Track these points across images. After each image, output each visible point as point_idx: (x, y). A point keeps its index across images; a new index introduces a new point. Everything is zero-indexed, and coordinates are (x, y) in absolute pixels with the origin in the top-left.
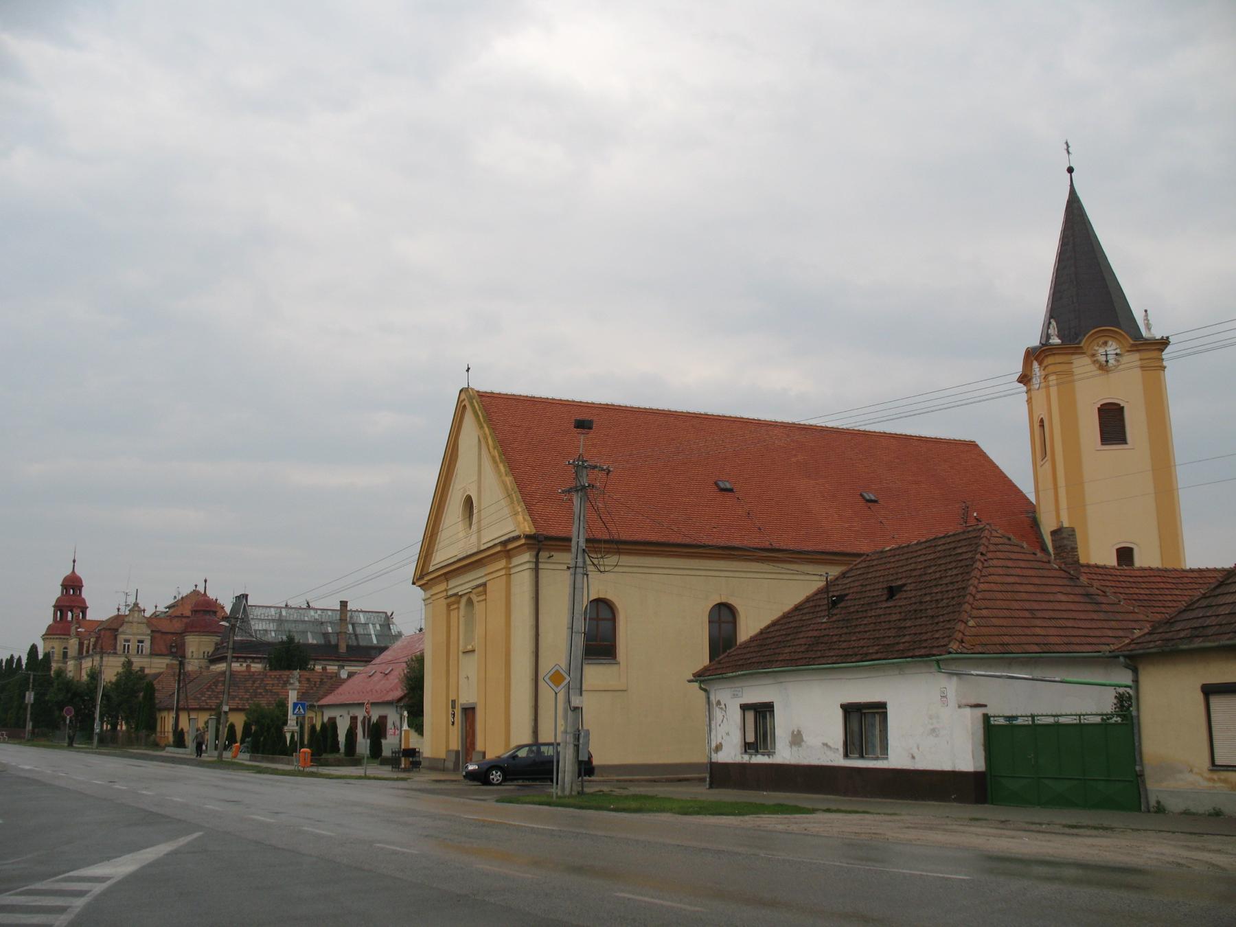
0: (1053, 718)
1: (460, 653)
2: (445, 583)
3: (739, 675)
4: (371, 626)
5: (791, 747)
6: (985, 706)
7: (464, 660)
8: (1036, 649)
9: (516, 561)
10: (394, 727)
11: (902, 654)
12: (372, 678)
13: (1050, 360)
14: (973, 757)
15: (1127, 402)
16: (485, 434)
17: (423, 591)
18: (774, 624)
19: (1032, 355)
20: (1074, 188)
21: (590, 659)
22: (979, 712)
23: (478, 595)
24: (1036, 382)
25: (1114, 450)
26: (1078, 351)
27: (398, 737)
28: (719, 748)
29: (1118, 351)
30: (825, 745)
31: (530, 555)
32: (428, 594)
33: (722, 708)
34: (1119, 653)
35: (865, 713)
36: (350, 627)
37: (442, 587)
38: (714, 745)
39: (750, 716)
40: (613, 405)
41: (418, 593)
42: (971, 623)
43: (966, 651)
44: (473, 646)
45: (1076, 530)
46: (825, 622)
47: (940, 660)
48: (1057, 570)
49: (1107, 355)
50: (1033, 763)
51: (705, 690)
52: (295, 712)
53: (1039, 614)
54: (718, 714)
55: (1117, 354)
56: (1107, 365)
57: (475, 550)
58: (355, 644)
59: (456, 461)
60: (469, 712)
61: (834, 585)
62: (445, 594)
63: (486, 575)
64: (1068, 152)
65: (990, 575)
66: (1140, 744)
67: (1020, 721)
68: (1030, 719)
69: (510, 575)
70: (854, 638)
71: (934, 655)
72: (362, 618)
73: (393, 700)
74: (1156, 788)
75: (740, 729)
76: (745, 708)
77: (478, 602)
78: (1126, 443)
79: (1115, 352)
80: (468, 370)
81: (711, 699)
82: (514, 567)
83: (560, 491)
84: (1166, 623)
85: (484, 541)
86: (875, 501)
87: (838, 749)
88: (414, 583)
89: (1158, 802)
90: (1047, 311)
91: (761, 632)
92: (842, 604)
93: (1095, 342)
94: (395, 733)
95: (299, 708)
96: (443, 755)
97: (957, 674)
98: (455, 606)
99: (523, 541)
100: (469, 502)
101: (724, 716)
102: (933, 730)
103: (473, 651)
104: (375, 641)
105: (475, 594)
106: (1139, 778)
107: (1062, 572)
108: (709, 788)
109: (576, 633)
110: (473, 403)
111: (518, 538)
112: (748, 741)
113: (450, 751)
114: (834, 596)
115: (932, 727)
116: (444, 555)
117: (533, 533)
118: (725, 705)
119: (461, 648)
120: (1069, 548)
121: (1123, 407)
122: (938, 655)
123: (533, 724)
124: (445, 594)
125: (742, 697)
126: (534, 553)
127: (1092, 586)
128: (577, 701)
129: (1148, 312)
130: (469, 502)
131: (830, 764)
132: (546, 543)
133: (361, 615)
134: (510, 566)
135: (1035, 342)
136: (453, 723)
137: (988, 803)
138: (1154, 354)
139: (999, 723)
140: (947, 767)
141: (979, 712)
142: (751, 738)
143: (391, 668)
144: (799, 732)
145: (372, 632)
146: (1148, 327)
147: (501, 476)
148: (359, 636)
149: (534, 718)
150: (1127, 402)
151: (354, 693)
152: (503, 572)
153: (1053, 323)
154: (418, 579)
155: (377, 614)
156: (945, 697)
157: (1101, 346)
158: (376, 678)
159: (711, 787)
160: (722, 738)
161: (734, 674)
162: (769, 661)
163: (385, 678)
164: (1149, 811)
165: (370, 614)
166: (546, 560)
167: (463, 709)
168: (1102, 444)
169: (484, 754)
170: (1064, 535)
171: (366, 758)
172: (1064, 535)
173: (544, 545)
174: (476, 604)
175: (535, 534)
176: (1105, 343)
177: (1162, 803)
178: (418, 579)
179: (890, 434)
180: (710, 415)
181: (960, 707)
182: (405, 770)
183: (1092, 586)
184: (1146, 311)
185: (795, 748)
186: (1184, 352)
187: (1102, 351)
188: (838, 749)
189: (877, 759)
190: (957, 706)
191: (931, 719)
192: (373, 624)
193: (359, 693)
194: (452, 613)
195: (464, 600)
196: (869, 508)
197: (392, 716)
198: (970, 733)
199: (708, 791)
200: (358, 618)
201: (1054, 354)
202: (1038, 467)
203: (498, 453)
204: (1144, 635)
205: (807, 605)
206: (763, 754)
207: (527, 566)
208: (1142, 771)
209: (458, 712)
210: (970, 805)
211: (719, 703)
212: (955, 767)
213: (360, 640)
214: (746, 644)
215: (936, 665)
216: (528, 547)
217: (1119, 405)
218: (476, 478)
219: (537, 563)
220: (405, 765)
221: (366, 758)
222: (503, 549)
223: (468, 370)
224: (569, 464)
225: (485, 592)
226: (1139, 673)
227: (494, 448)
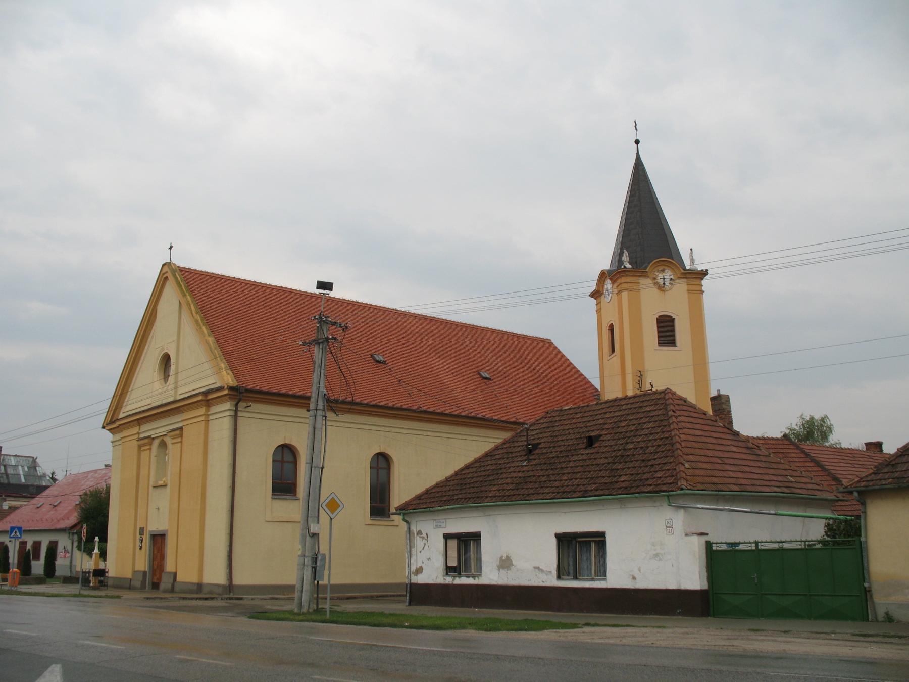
0: (778, 544)
1: (151, 488)
2: (138, 427)
3: (448, 509)
4: (20, 468)
5: (499, 570)
6: (707, 534)
7: (154, 493)
8: (737, 488)
9: (215, 409)
10: (65, 550)
11: (627, 490)
12: (40, 509)
13: (623, 280)
14: (700, 578)
15: (677, 315)
16: (189, 301)
17: (112, 435)
18: (467, 467)
19: (603, 275)
21: (277, 495)
22: (704, 539)
23: (173, 438)
24: (606, 298)
25: (667, 350)
26: (644, 275)
27: (69, 560)
28: (419, 571)
29: (672, 277)
30: (538, 568)
31: (231, 404)
32: (118, 436)
33: (423, 538)
34: (854, 489)
35: (579, 541)
36: (2, 468)
37: (135, 430)
38: (414, 568)
39: (453, 544)
40: (286, 288)
41: (108, 436)
42: (687, 465)
43: (692, 488)
44: (164, 482)
45: (730, 398)
46: (525, 466)
47: (671, 495)
48: (722, 427)
49: (664, 279)
50: (756, 582)
51: (407, 522)
52: (12, 536)
53: (726, 461)
54: (419, 542)
55: (671, 279)
56: (664, 287)
57: (171, 399)
58: (6, 482)
59: (153, 324)
60: (159, 539)
61: (520, 436)
62: (136, 437)
64: (636, 129)
65: (684, 428)
66: (868, 565)
67: (742, 547)
68: (754, 545)
69: (208, 421)
70: (566, 478)
71: (664, 491)
72: (13, 462)
73: (66, 527)
74: (882, 601)
75: (443, 555)
76: (447, 537)
77: (173, 443)
78: (675, 346)
79: (670, 278)
80: (171, 248)
81: (411, 529)
82: (213, 414)
83: (301, 342)
84: (887, 465)
85: (181, 391)
86: (489, 379)
87: (551, 572)
88: (103, 427)
89: (887, 614)
90: (616, 245)
91: (456, 474)
92: (537, 451)
93: (656, 269)
94: (65, 557)
95: (16, 532)
96: (128, 574)
97: (683, 507)
98: (148, 447)
99: (226, 392)
100: (166, 360)
101: (425, 544)
102: (656, 555)
103: (165, 486)
104: (23, 480)
105: (170, 437)
106: (868, 593)
107: (726, 429)
108: (409, 606)
109: (315, 467)
110: (176, 275)
111: (221, 389)
112: (449, 565)
113: (137, 571)
114: (530, 445)
115: (655, 552)
116: (135, 403)
117: (235, 385)
118: (427, 534)
119: (151, 483)
120: (726, 411)
121: (674, 319)
122: (670, 491)
123: (228, 550)
124: (136, 437)
125: (445, 527)
126: (234, 403)
127: (749, 442)
128: (316, 529)
129: (693, 250)
130: (166, 360)
131: (541, 584)
132: (245, 394)
133: (12, 458)
134: (209, 413)
135: (606, 266)
136: (141, 548)
137: (711, 616)
138: (696, 282)
139: (722, 549)
140: (672, 586)
141: (704, 539)
142: (453, 562)
143: (59, 501)
144: (508, 558)
145: (21, 472)
146: (692, 261)
147: (204, 337)
148: (10, 476)
149: (229, 544)
150: (677, 315)
151: (23, 521)
152: (202, 418)
153: (626, 252)
154: (109, 424)
155: (26, 458)
156: (671, 527)
157: (660, 273)
158: (44, 510)
159: (410, 604)
160: (423, 563)
161: (443, 508)
162: (478, 497)
163: (54, 509)
164: (877, 621)
165: (20, 458)
166: (244, 410)
167: (151, 535)
168: (659, 345)
169: (175, 575)
170: (723, 401)
172: (723, 401)
173: (243, 396)
174: (170, 446)
175: (237, 386)
176: (663, 271)
177: (890, 613)
178: (109, 424)
179: (491, 329)
180: (360, 303)
181: (686, 535)
182: (94, 588)
183: (749, 442)
184: (691, 250)
185: (503, 572)
186: (899, 246)
187: (660, 276)
188: (551, 572)
189: (593, 580)
190: (684, 534)
191: (654, 546)
192: (22, 466)
193: (28, 521)
194: (143, 453)
195: (156, 442)
196: (486, 384)
197: (64, 542)
198: (697, 557)
199: (407, 607)
200: (10, 461)
202: (605, 360)
203: (200, 317)
204: (870, 475)
205: (497, 452)
206: (468, 577)
207: (228, 413)
208: (870, 587)
210: (695, 618)
211: (420, 533)
212: (680, 586)
213: (10, 479)
215: (667, 500)
216: (230, 397)
217: (671, 317)
218: (175, 338)
219: (236, 411)
220: (95, 583)
222: (204, 398)
223: (171, 248)
224: (315, 318)
225: (181, 436)
226: (867, 505)
227: (197, 313)
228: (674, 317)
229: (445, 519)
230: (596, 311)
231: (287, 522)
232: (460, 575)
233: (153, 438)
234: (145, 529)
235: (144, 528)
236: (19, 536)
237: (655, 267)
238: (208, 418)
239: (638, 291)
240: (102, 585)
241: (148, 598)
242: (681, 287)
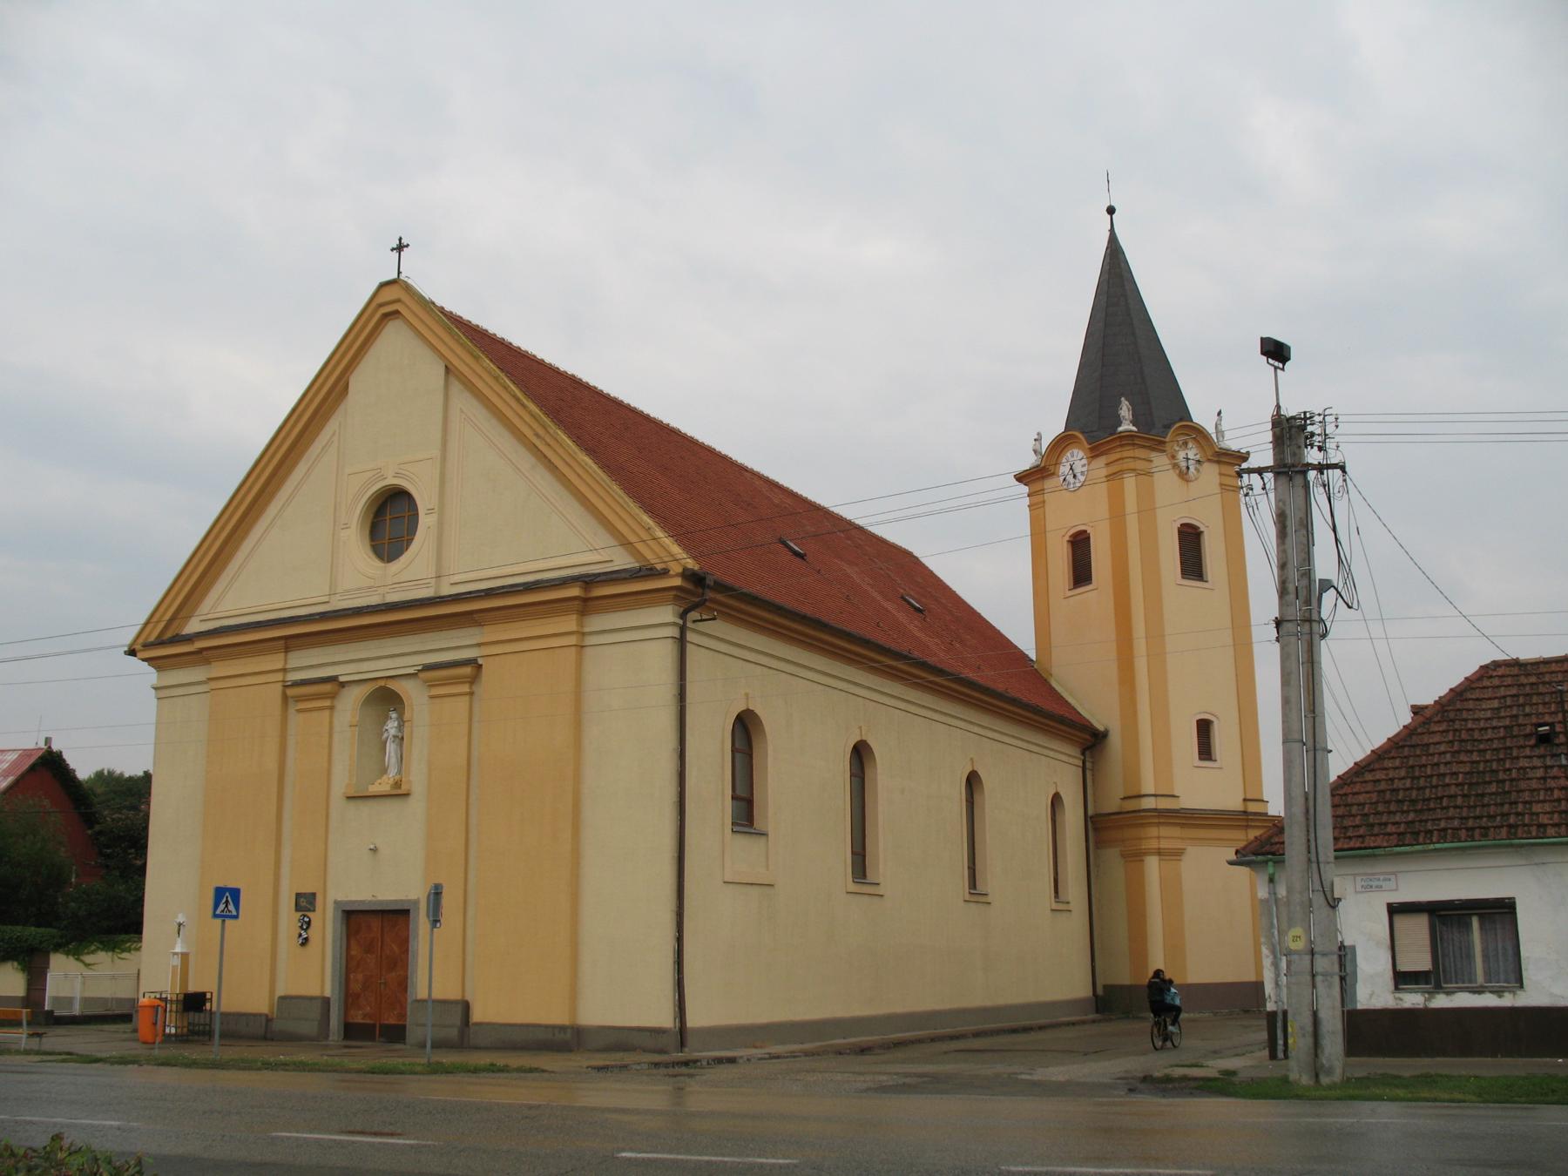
15: (1207, 527)
20: (1115, 234)
26: (1158, 446)
37: (274, 661)
52: (218, 912)
56: (1187, 473)
62: (280, 677)
63: (479, 645)
76: (1394, 910)
95: (227, 902)
98: (327, 703)
99: (678, 582)
105: (425, 681)
112: (1402, 967)
121: (1202, 532)
125: (1396, 890)
150: (1207, 527)
152: (573, 640)
167: (344, 911)
168: (1183, 578)
169: (466, 1007)
171: (25, 1023)
201: (1134, 444)
209: (326, 925)
214: (1286, 813)
216: (678, 594)
219: (683, 630)
221: (25, 1023)
228: (1202, 529)
229: (1394, 873)
230: (1029, 506)
231: (752, 884)
232: (1438, 988)
233: (342, 683)
234: (319, 898)
235: (314, 895)
236: (234, 913)
237: (1182, 434)
238: (583, 640)
239: (1149, 474)
240: (196, 1034)
241: (599, 1069)
242: (1210, 475)
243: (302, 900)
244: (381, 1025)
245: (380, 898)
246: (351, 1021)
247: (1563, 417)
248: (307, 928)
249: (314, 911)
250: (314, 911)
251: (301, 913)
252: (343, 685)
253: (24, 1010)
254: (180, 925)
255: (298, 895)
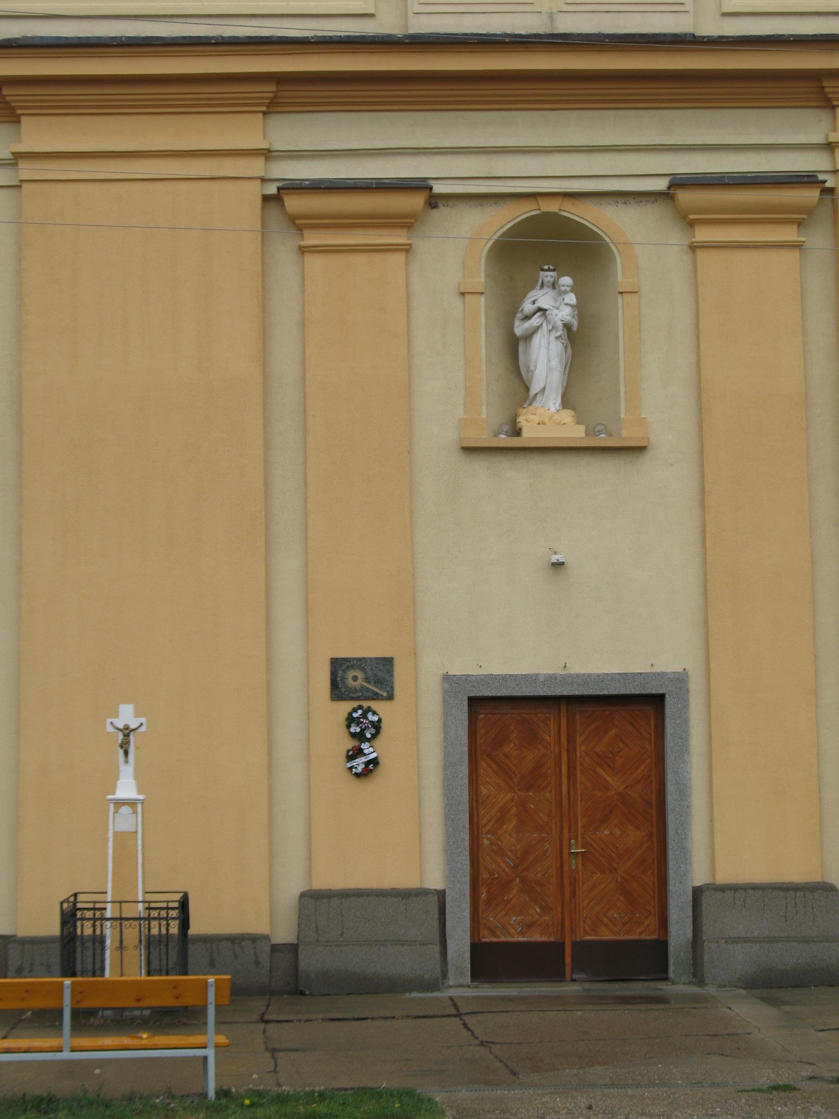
62: (256, 167)
235: (388, 662)
243: (351, 674)
244: (574, 944)
245: (577, 668)
246: (487, 939)
247: (2, 162)
248: (374, 736)
249: (390, 697)
250: (390, 697)
251: (348, 706)
252: (434, 201)
253: (68, 982)
254: (127, 732)
255: (338, 666)
